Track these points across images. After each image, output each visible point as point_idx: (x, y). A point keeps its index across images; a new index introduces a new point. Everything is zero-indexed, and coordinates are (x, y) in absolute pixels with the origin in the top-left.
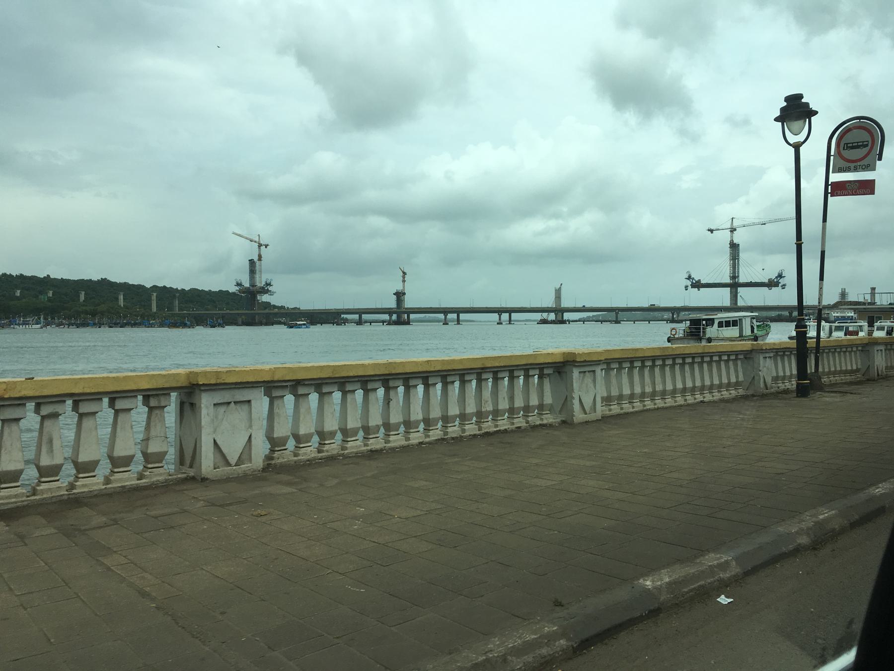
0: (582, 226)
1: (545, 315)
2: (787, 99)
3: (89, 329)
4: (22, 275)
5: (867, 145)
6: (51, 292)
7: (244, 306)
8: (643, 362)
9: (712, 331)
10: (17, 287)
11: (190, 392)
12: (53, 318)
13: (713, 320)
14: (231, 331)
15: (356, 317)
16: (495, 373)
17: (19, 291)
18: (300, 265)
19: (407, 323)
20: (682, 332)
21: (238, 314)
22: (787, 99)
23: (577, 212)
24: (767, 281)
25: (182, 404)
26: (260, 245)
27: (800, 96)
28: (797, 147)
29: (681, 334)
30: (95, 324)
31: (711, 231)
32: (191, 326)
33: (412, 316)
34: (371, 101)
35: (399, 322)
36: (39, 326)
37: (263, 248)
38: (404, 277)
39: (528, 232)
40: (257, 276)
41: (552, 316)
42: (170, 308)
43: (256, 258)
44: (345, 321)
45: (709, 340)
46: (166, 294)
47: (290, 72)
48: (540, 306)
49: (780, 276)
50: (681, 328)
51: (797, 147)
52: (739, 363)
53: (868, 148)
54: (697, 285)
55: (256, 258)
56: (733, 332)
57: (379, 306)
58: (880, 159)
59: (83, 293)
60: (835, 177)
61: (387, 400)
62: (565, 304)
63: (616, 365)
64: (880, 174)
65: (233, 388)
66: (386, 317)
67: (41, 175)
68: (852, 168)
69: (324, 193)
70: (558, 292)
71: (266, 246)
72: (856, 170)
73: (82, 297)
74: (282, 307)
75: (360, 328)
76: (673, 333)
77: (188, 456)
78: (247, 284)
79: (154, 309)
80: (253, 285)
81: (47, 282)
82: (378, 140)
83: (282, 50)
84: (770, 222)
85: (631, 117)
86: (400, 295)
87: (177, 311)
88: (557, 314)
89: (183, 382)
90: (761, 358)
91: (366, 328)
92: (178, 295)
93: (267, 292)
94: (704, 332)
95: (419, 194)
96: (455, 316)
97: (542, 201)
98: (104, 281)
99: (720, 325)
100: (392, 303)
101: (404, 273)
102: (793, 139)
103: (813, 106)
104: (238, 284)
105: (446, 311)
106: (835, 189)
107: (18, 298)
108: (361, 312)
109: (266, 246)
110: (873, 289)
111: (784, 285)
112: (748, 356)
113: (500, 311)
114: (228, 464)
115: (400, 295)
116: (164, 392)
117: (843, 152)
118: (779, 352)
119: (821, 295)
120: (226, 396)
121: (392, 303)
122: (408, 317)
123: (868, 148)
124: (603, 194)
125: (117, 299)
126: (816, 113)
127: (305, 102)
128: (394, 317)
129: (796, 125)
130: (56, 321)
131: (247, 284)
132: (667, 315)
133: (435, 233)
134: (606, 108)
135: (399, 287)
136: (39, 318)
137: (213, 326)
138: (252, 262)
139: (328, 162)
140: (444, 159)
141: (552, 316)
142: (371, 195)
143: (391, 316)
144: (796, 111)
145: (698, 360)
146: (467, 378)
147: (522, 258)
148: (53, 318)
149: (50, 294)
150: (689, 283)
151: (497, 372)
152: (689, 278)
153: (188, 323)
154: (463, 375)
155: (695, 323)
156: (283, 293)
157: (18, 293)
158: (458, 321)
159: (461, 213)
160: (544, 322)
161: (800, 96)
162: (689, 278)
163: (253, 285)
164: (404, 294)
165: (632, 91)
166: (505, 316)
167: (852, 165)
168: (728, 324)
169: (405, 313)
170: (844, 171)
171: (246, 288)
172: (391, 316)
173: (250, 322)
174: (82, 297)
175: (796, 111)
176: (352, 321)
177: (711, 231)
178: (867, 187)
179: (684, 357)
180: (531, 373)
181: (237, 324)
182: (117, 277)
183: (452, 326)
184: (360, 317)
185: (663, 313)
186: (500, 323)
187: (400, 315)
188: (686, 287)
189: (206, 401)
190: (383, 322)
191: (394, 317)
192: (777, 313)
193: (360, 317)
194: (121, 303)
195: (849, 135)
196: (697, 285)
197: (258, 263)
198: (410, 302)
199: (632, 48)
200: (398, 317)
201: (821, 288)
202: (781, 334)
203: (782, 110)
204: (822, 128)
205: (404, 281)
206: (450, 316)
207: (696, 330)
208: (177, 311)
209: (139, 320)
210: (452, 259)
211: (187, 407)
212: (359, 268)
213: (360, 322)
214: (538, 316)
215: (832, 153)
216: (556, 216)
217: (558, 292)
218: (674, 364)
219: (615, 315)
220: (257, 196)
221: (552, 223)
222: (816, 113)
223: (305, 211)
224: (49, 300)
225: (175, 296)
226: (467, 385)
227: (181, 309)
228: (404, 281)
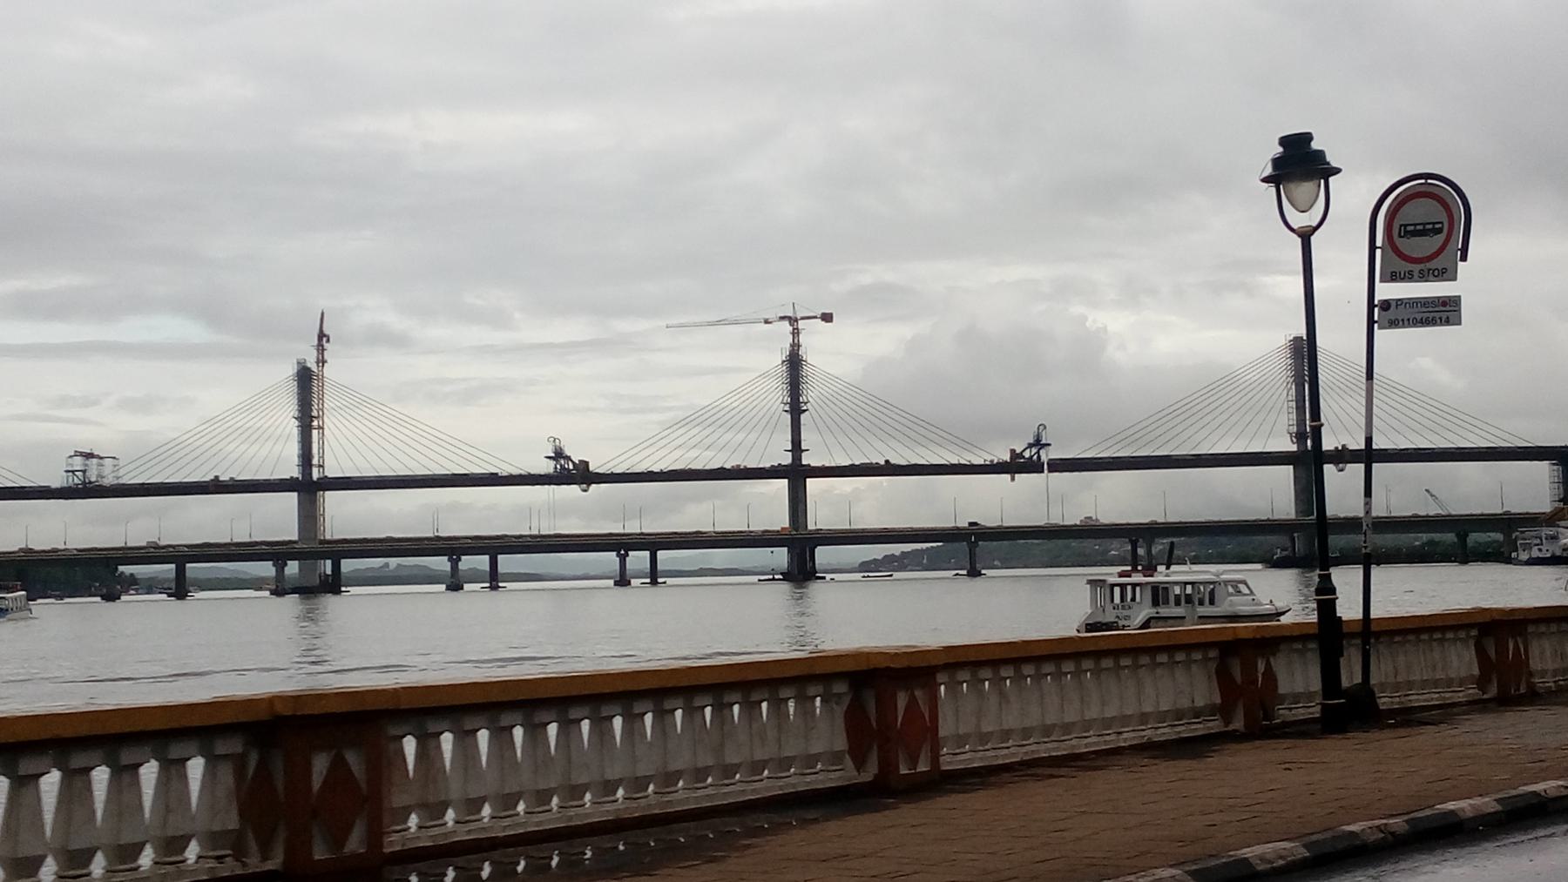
2: (1285, 141)
5: (1440, 231)
22: (1285, 141)
27: (1306, 138)
28: (1306, 236)
33: (348, 565)
44: (132, 584)
51: (1306, 236)
53: (1441, 238)
57: (242, 537)
58: (1464, 258)
60: (1385, 291)
64: (1468, 283)
68: (1416, 274)
72: (1423, 277)
96: (482, 562)
102: (1298, 220)
103: (1333, 160)
106: (1382, 315)
110: (654, 582)
117: (1399, 242)
119: (1368, 504)
122: (336, 567)
123: (1441, 238)
126: (1337, 171)
129: (1304, 189)
132: (1119, 547)
143: (280, 569)
144: (1299, 164)
161: (1306, 138)
167: (1416, 268)
169: (324, 556)
170: (1402, 280)
172: (280, 569)
175: (1299, 164)
176: (150, 586)
178: (1444, 312)
184: (181, 572)
185: (1107, 542)
186: (623, 581)
191: (292, 568)
192: (1425, 537)
193: (181, 572)
195: (1406, 208)
203: (1276, 162)
204: (1355, 196)
206: (468, 562)
215: (1379, 243)
219: (970, 548)
222: (1337, 171)
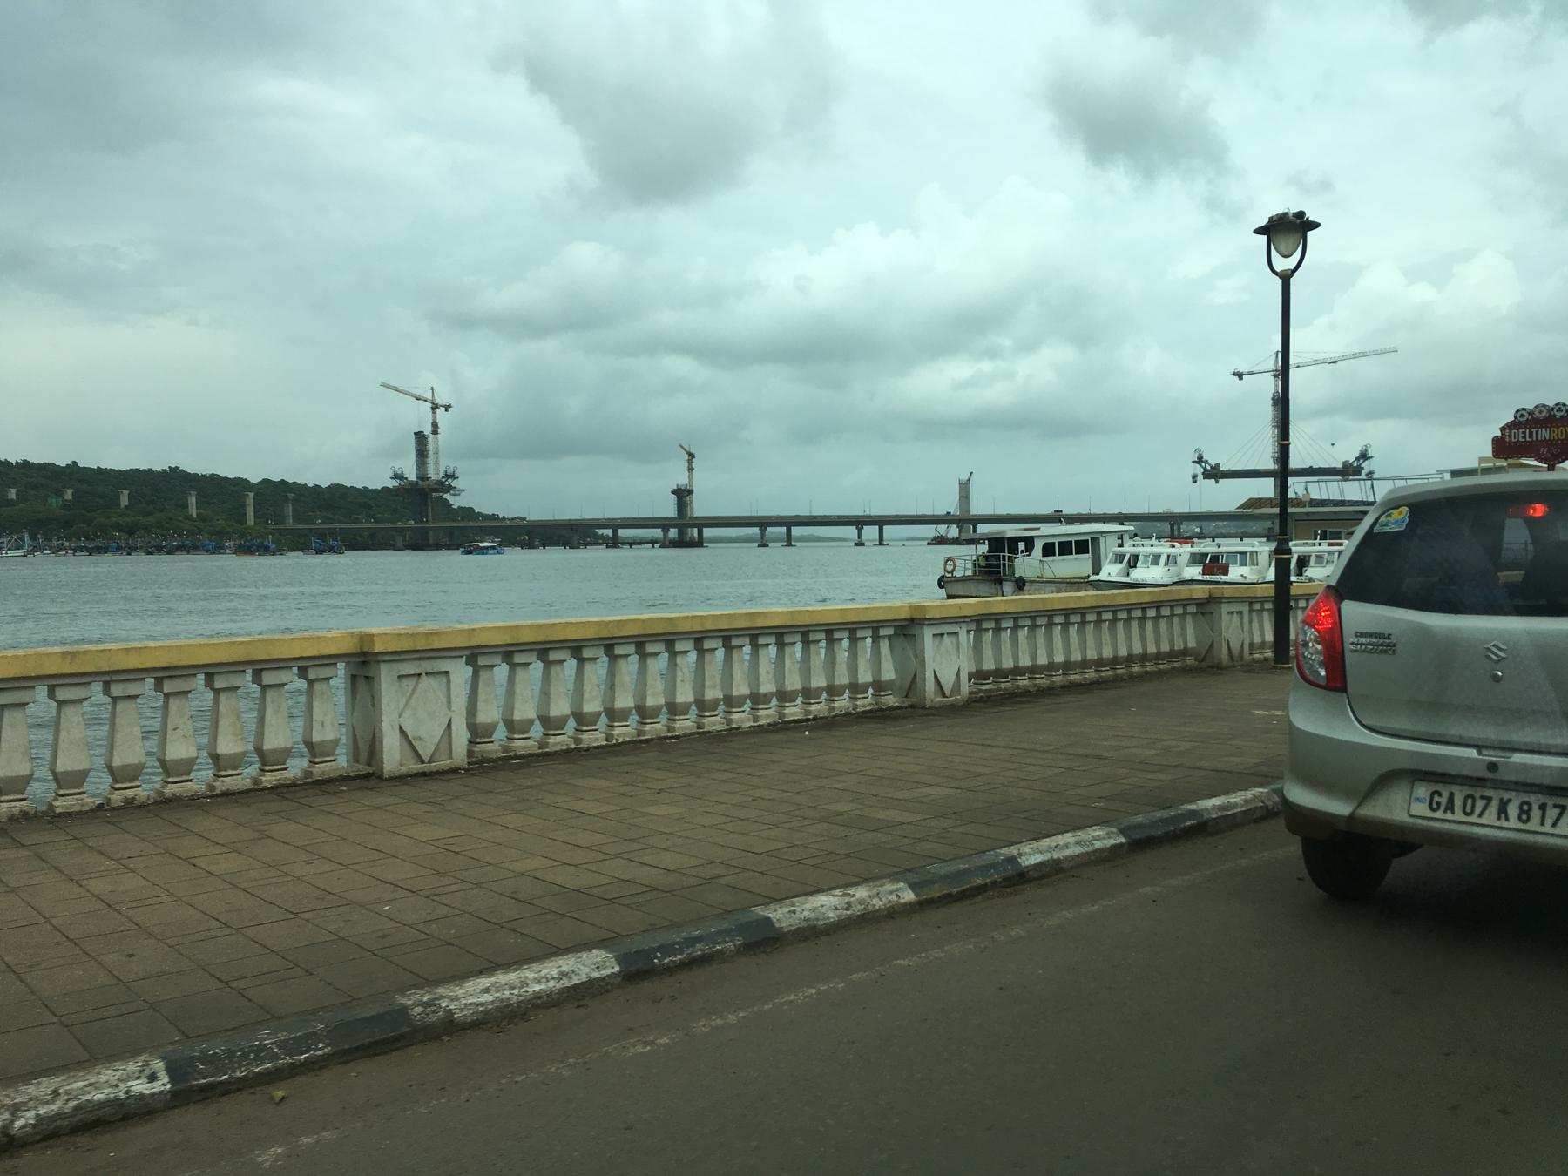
0: (1038, 371)
1: (942, 529)
3: (108, 557)
4: (26, 462)
6: (70, 492)
7: (414, 514)
8: (1067, 616)
9: (1028, 565)
10: (14, 484)
11: (363, 663)
12: (48, 539)
13: (1030, 542)
14: (349, 558)
15: (609, 532)
16: (853, 632)
17: (14, 491)
18: (539, 440)
19: (699, 543)
20: (970, 565)
21: (396, 529)
23: (1029, 346)
24: (1339, 465)
25: (354, 677)
26: (435, 407)
29: (964, 569)
30: (119, 549)
31: (1240, 375)
32: (279, 551)
33: (708, 532)
34: (660, 153)
35: (682, 543)
36: (20, 552)
37: (440, 411)
38: (690, 462)
39: (943, 382)
40: (431, 461)
41: (954, 531)
42: (280, 519)
43: (427, 430)
45: (1020, 584)
46: (275, 493)
47: (517, 104)
48: (930, 513)
49: (1364, 456)
50: (966, 558)
52: (1189, 620)
54: (1214, 473)
55: (427, 430)
56: (1076, 566)
59: (126, 493)
61: (853, 655)
62: (977, 509)
63: (1044, 621)
65: (424, 656)
66: (657, 533)
67: (87, 289)
69: (581, 318)
70: (965, 487)
71: (447, 408)
73: (124, 500)
74: (494, 517)
75: (613, 553)
76: (949, 568)
77: (912, 685)
78: (412, 475)
79: (251, 520)
80: (423, 477)
81: (73, 474)
82: (676, 224)
83: (502, 63)
84: (1345, 358)
85: (1119, 177)
86: (683, 494)
87: (290, 523)
88: (684, 529)
89: (347, 647)
90: (1225, 617)
91: (624, 553)
92: (291, 495)
93: (449, 489)
94: (1012, 566)
95: (751, 316)
97: (968, 327)
98: (175, 471)
99: (1048, 550)
100: (669, 509)
101: (691, 456)
104: (397, 476)
105: (763, 523)
107: (10, 503)
108: (616, 525)
109: (447, 408)
111: (1371, 473)
112: (1206, 607)
113: (859, 522)
114: (944, 695)
115: (683, 494)
116: (329, 660)
118: (1247, 599)
120: (409, 668)
121: (669, 509)
122: (700, 533)
124: (1074, 315)
125: (185, 506)
127: (544, 157)
128: (673, 533)
130: (55, 543)
131: (412, 475)
133: (779, 387)
134: (1073, 161)
135: (682, 480)
136: (22, 539)
137: (319, 552)
138: (420, 438)
139: (589, 260)
140: (792, 255)
141: (954, 531)
142: (667, 319)
145: (1137, 613)
146: (788, 639)
147: (931, 427)
148: (48, 539)
149: (69, 495)
150: (1199, 470)
151: (782, 634)
152: (1200, 460)
153: (273, 546)
154: (782, 634)
155: (997, 544)
156: (482, 490)
157: (12, 494)
158: (789, 540)
159: (825, 350)
160: (940, 541)
162: (1200, 460)
163: (423, 477)
164: (691, 492)
165: (1121, 132)
166: (870, 532)
168: (1065, 548)
169: (693, 526)
171: (411, 483)
173: (419, 543)
174: (124, 500)
177: (1240, 375)
179: (1083, 612)
180: (860, 634)
181: (395, 548)
182: (195, 465)
183: (871, 551)
186: (860, 544)
187: (684, 529)
188: (1195, 477)
189: (386, 677)
190: (653, 542)
191: (673, 533)
194: (193, 511)
196: (1214, 473)
197: (431, 438)
198: (701, 507)
199: (1120, 54)
200: (681, 533)
201: (409, 394)
202: (1252, 567)
205: (690, 469)
207: (998, 560)
208: (290, 523)
209: (446, 540)
210: (810, 432)
211: (361, 683)
212: (640, 447)
213: (615, 543)
214: (929, 531)
216: (992, 354)
217: (965, 487)
218: (1115, 620)
220: (463, 321)
221: (987, 366)
223: (551, 350)
224: (66, 505)
225: (286, 499)
226: (860, 644)
227: (297, 519)
228: (690, 469)
